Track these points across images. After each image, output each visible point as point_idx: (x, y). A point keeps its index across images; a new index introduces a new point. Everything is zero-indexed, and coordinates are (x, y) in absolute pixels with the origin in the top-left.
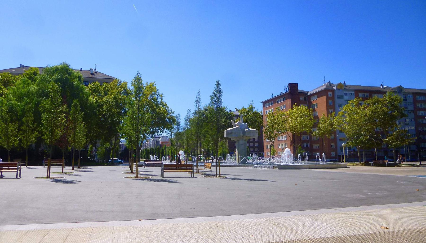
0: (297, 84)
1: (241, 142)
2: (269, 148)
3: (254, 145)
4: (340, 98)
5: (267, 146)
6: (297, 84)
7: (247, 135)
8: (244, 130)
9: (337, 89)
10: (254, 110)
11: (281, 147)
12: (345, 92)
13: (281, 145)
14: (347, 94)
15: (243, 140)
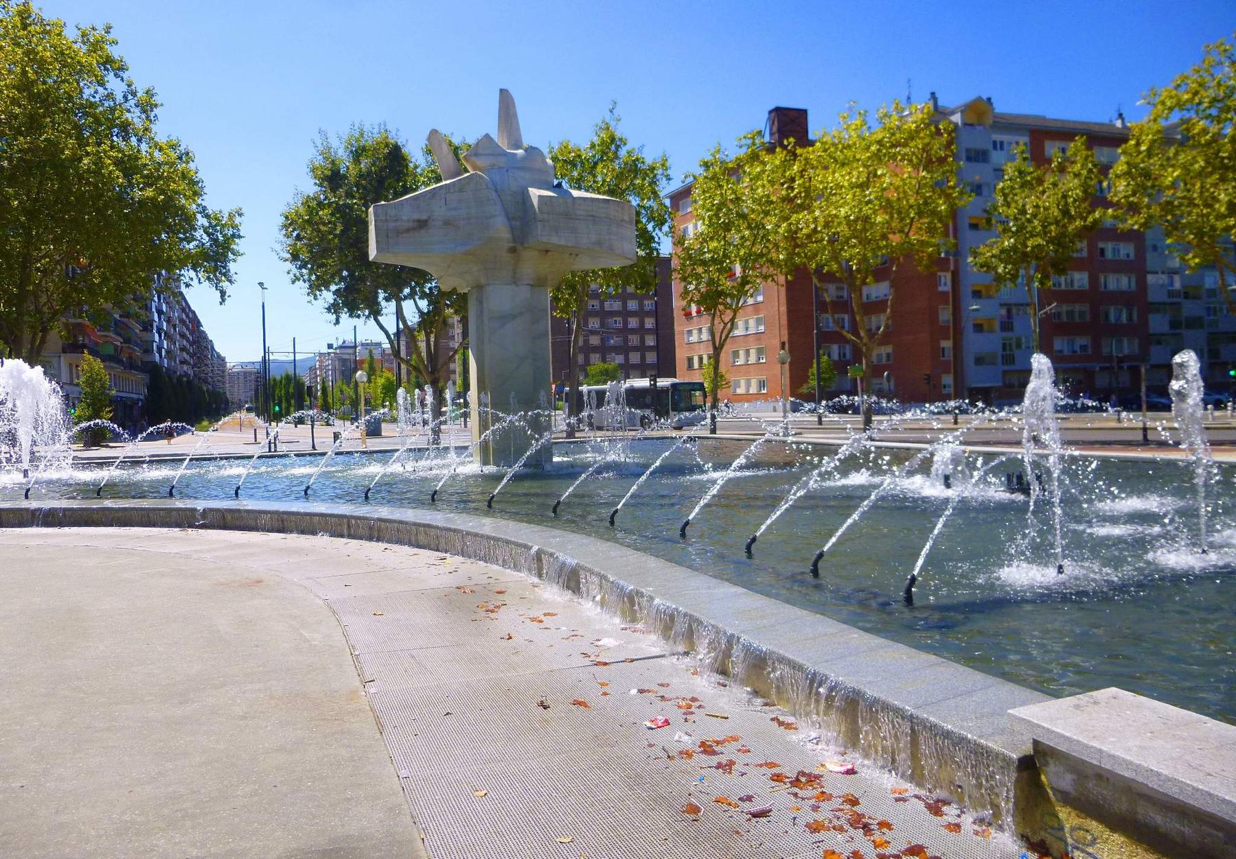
0: (805, 112)
1: (502, 298)
2: (696, 365)
3: (643, 358)
4: (977, 161)
5: (690, 360)
6: (805, 112)
7: (542, 235)
8: (526, 197)
9: (965, 124)
10: (623, 152)
11: (741, 361)
12: (998, 137)
13: (742, 353)
14: (1002, 143)
15: (515, 281)
